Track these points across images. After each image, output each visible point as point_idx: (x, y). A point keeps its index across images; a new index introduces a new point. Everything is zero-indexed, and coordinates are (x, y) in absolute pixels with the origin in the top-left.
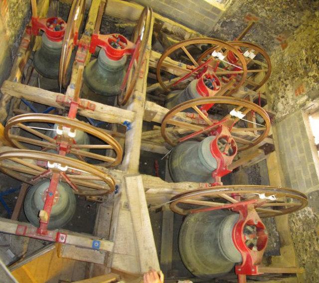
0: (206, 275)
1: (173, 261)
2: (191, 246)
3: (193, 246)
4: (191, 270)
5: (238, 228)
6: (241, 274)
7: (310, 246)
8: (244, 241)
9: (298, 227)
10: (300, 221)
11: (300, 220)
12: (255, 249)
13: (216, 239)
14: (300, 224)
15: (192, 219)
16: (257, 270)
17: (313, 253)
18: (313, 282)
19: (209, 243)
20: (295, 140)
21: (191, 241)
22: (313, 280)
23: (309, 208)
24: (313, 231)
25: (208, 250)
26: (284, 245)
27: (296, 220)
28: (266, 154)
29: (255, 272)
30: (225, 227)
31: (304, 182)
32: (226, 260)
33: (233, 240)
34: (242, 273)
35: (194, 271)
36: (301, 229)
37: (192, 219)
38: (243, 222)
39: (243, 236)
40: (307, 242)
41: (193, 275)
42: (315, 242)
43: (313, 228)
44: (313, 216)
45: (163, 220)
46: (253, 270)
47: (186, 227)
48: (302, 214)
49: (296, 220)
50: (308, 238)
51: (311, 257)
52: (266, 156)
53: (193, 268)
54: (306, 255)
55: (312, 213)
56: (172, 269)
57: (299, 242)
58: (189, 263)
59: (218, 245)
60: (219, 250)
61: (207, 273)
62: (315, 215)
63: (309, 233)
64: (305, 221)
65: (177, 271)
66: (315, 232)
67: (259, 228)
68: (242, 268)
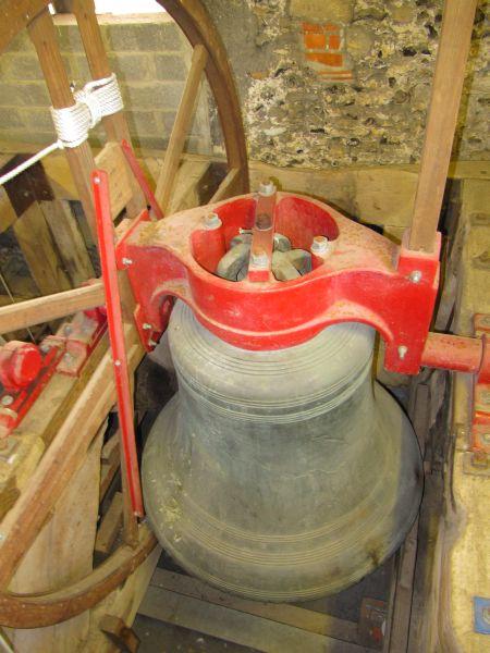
0: (397, 509)
1: (330, 614)
2: (271, 548)
3: (274, 538)
4: (367, 567)
5: (215, 302)
6: (422, 347)
7: (372, 121)
8: (269, 286)
9: (306, 151)
10: (290, 140)
11: (286, 138)
12: (322, 248)
13: (252, 430)
14: (298, 141)
15: (171, 515)
16: (421, 254)
17: (397, 118)
18: (486, 143)
19: (268, 467)
20: (25, 83)
21: (251, 545)
22: (479, 141)
23: (251, 91)
24: (329, 99)
25: (297, 477)
26: (351, 201)
27: (284, 152)
28: (49, 197)
29: (426, 267)
30: (203, 371)
31: (164, 83)
32: (351, 404)
33: (266, 344)
34: (417, 347)
35: (373, 555)
36: (313, 140)
37: (171, 515)
38: (197, 282)
39: (247, 286)
40: (361, 130)
41: (388, 560)
42: (365, 99)
43: (320, 92)
44: (279, 81)
45: (177, 621)
46: (417, 277)
47: (192, 549)
48: (269, 125)
49: (284, 152)
50: (346, 123)
51: (408, 130)
52: (58, 197)
53: (359, 559)
54: (399, 144)
55: (270, 82)
56: (356, 620)
57: (355, 159)
58: (336, 573)
59: (278, 427)
60: (300, 425)
61: (393, 501)
62: (277, 75)
63: (332, 114)
64: (292, 120)
65: (367, 604)
66: (333, 89)
67: (240, 217)
68: (399, 341)
